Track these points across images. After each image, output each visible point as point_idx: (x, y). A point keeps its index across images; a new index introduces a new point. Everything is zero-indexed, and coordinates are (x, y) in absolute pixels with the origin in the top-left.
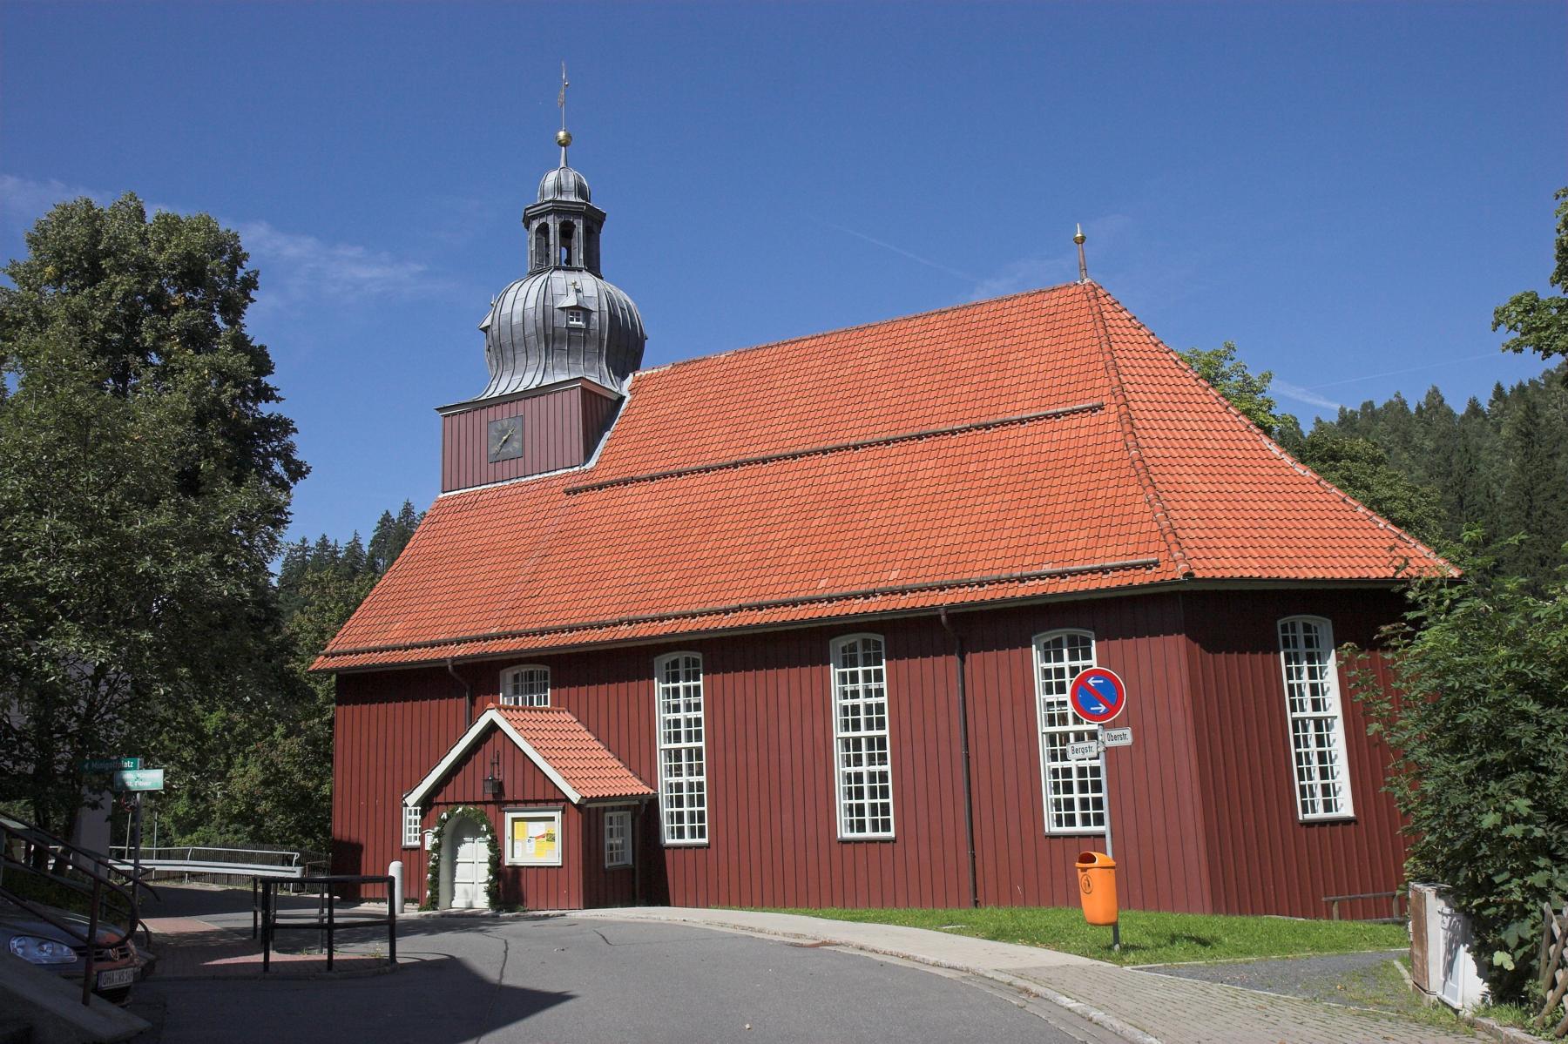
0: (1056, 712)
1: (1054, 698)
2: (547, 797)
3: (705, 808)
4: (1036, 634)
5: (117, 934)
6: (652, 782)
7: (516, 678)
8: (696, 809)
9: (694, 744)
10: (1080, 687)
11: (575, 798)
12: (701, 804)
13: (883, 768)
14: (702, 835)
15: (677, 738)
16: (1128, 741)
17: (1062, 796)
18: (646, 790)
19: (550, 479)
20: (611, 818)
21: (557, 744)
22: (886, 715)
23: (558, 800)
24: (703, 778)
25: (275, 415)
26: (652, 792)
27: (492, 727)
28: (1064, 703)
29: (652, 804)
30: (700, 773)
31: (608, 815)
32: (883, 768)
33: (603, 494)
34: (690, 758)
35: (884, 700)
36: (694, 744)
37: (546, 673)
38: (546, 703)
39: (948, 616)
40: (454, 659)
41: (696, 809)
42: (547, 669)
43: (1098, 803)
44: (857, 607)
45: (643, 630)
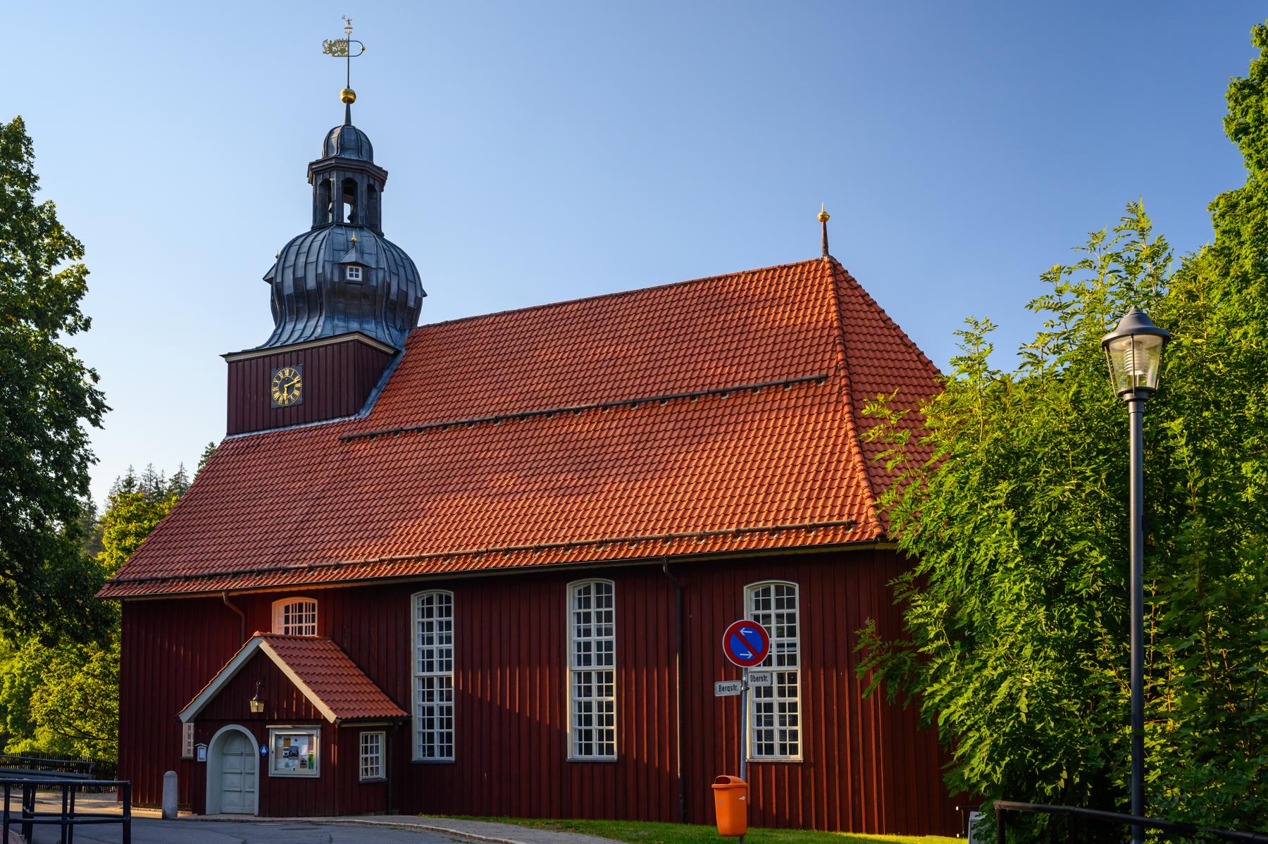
0: (786, 653)
1: (786, 640)
2: (307, 716)
3: (453, 730)
4: (747, 584)
5: (332, 273)
6: (406, 704)
7: (287, 609)
8: (445, 730)
9: (445, 673)
10: (734, 636)
11: (331, 717)
12: (449, 726)
13: (793, 699)
14: (449, 754)
15: (588, 661)
16: (717, 685)
17: (763, 728)
18: (400, 713)
19: (327, 426)
20: (366, 737)
21: (319, 670)
22: (614, 652)
23: (319, 720)
24: (452, 703)
25: (76, 356)
26: (405, 714)
27: (259, 653)
28: (794, 645)
29: (407, 722)
30: (449, 699)
31: (362, 734)
32: (793, 699)
33: (374, 443)
34: (600, 680)
35: (613, 638)
36: (445, 673)
37: (314, 605)
38: (313, 633)
39: (669, 566)
40: (228, 591)
41: (445, 730)
42: (316, 602)
43: (794, 735)
44: (590, 555)
45: (402, 571)
